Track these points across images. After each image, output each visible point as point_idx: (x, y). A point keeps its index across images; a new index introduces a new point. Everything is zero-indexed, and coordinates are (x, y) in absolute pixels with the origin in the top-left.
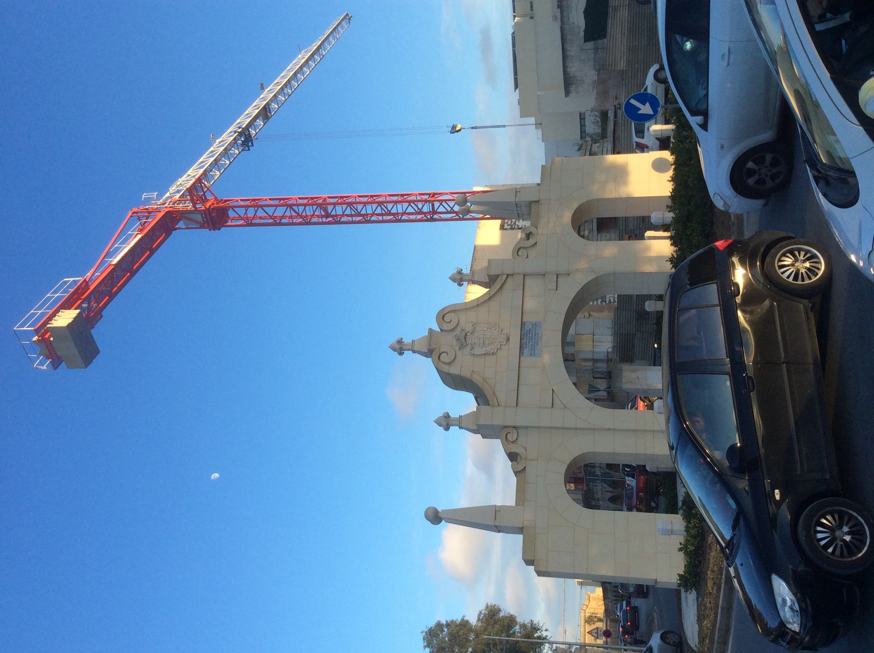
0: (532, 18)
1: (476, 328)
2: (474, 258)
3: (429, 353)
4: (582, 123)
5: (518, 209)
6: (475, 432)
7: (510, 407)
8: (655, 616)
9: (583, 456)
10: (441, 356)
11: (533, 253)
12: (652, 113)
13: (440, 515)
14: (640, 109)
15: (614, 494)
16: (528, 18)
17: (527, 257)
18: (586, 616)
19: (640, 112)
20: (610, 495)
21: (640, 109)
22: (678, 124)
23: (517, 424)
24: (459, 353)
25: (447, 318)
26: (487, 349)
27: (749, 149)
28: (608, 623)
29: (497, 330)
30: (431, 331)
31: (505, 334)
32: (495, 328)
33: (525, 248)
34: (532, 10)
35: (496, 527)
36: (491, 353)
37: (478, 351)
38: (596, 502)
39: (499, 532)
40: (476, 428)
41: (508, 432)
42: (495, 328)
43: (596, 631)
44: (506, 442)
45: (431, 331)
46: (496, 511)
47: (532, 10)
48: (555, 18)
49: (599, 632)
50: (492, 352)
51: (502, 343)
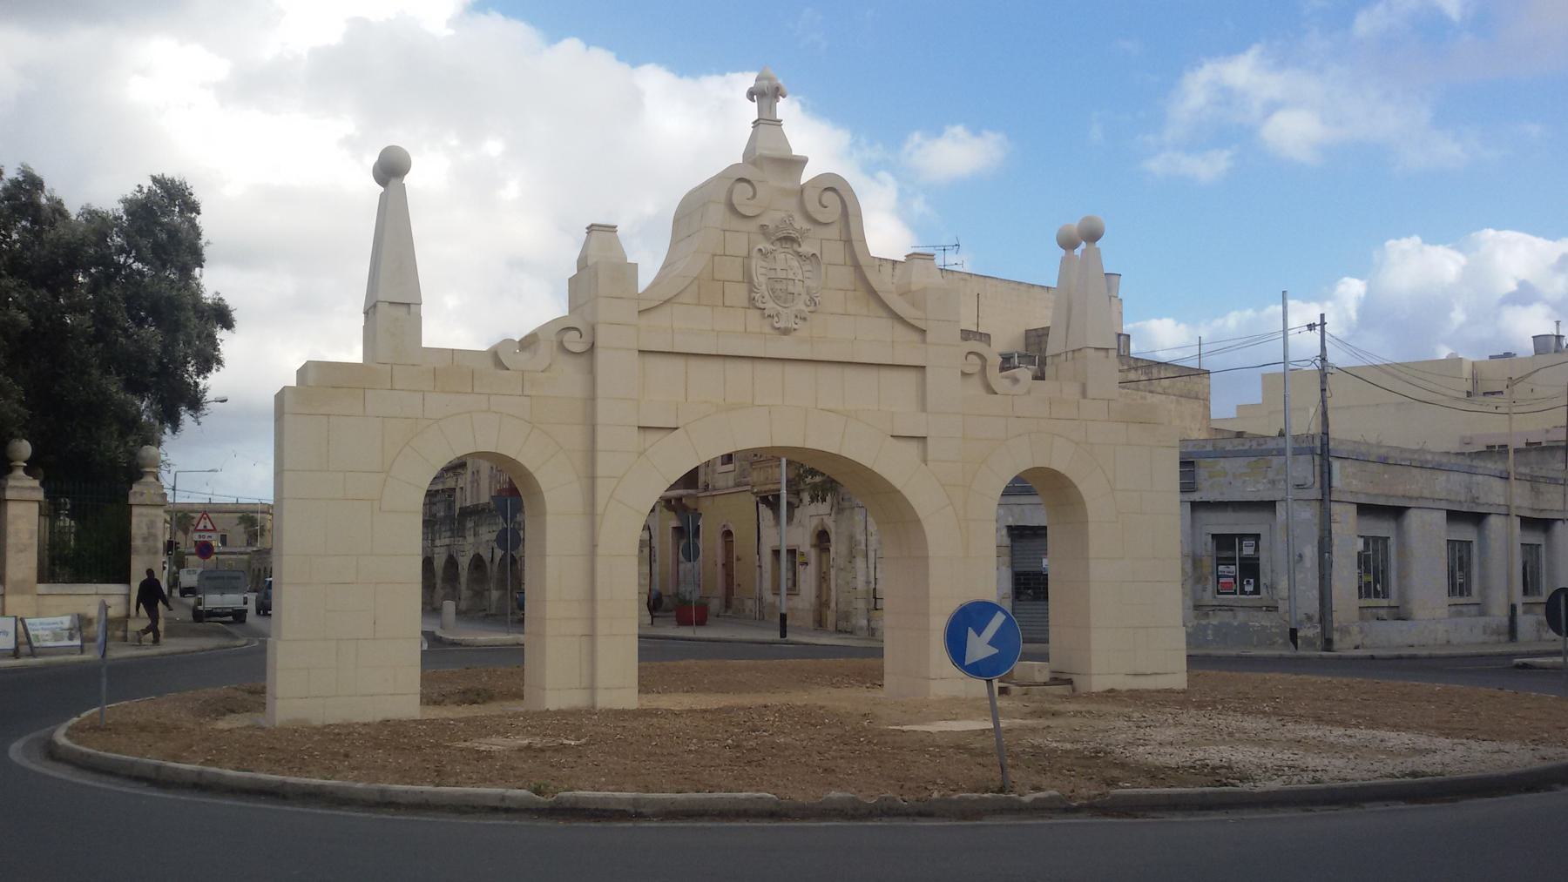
0: (1469, 394)
1: (808, 262)
2: (968, 277)
3: (753, 156)
4: (1326, 439)
5: (1070, 355)
6: (582, 263)
7: (686, 373)
8: (243, 642)
9: (537, 493)
10: (745, 184)
11: (975, 388)
12: (966, 663)
13: (393, 182)
14: (979, 632)
15: (488, 565)
16: (1468, 386)
17: (964, 374)
18: (255, 515)
19: (971, 631)
20: (487, 556)
21: (979, 633)
22: (176, 313)
23: (601, 356)
24: (752, 226)
25: (829, 198)
26: (764, 287)
27: (746, 73)
28: (246, 557)
29: (804, 308)
30: (801, 162)
31: (796, 326)
32: (809, 303)
33: (984, 368)
34: (1485, 394)
35: (375, 306)
36: (754, 294)
37: (757, 264)
38: (472, 530)
39: (366, 313)
40: (590, 263)
41: (583, 332)
42: (809, 303)
43: (210, 527)
44: (562, 329)
45: (801, 162)
46: (409, 304)
47: (1485, 394)
48: (1468, 440)
49: (207, 534)
50: (757, 296)
51: (776, 319)
